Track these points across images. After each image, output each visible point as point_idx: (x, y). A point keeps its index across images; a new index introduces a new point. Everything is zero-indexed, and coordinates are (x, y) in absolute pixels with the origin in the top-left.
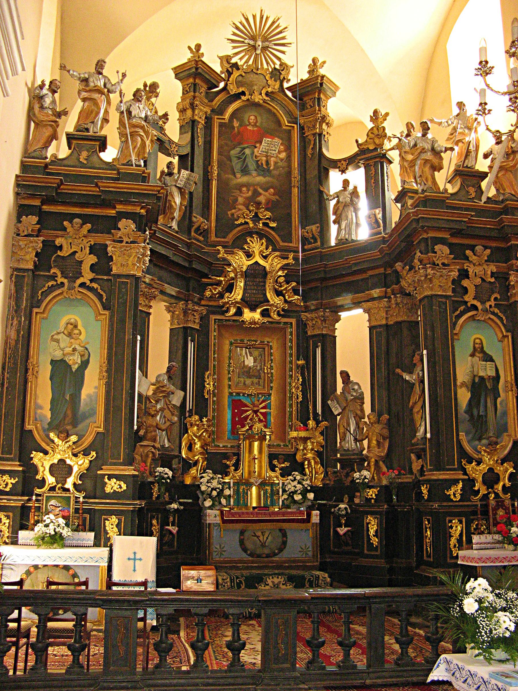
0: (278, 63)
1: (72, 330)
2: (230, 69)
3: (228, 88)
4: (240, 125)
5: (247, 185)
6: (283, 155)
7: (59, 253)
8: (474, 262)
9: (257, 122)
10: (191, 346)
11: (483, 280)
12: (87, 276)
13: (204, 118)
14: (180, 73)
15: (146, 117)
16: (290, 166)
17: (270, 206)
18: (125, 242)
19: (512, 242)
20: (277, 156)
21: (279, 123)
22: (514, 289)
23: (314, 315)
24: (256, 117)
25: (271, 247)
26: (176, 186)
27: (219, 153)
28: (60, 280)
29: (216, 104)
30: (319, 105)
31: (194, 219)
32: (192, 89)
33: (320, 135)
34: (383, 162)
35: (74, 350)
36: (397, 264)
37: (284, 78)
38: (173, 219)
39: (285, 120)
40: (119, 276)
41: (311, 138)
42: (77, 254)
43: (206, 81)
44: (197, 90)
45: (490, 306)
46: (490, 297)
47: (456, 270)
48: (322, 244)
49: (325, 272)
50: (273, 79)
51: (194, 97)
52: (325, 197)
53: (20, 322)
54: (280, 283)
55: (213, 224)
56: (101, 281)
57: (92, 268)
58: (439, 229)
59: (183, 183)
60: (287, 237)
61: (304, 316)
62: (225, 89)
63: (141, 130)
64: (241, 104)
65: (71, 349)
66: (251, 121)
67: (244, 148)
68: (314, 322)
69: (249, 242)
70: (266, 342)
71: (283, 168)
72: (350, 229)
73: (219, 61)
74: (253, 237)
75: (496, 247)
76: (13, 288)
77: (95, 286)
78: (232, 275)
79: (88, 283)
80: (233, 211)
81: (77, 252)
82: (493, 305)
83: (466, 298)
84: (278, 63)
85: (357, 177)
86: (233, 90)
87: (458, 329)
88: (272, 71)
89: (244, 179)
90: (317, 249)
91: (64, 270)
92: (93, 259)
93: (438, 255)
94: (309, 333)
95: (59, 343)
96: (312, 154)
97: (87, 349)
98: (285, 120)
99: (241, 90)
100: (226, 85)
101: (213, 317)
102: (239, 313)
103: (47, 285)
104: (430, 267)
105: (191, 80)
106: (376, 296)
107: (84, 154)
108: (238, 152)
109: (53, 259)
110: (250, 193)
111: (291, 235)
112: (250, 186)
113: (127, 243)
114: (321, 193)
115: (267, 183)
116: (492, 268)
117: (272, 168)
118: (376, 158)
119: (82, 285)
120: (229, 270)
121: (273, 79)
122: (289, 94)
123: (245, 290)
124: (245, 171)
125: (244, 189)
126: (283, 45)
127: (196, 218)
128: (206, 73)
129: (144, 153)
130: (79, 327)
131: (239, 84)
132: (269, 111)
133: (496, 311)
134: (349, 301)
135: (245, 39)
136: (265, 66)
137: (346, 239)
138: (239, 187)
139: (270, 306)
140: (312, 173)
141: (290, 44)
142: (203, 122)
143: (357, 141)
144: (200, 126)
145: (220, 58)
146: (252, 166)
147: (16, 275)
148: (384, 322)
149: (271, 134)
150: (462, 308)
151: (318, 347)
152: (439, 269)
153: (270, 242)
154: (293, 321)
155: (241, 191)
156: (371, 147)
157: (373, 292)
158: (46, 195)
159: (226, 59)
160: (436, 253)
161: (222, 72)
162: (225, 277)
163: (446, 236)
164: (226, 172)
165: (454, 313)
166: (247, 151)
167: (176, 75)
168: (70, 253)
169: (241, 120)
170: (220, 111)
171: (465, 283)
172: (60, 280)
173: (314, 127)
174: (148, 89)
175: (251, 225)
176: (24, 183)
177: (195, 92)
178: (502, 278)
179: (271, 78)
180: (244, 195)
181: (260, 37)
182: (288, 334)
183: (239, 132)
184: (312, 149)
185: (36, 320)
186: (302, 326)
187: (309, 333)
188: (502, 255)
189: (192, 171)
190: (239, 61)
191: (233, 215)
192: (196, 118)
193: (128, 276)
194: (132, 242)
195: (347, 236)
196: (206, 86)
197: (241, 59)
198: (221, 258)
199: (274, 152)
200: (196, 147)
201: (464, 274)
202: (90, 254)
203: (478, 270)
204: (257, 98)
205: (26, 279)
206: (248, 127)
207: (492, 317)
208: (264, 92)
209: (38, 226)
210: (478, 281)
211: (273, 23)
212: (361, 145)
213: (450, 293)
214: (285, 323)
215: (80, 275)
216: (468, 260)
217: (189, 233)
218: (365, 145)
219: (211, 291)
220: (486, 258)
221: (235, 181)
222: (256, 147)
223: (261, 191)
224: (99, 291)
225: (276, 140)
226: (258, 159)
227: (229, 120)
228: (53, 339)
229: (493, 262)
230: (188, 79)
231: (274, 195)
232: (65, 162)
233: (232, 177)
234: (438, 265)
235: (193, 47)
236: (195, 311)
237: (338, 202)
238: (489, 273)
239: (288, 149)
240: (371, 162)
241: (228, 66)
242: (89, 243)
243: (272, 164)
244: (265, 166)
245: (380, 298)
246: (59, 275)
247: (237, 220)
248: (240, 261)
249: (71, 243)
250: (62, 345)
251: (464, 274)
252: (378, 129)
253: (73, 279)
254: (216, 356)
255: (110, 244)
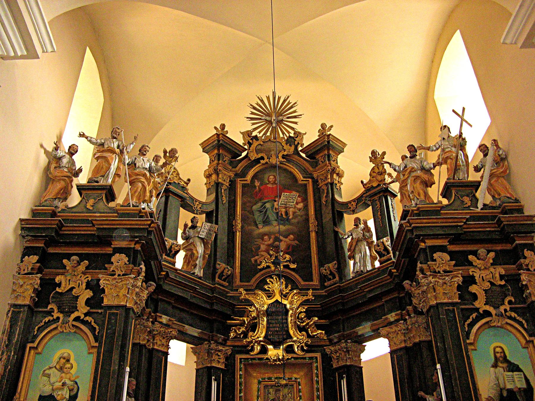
0: (292, 132)
1: (64, 364)
2: (251, 141)
3: (249, 155)
4: (261, 184)
5: (269, 234)
6: (301, 205)
7: (57, 289)
8: (479, 266)
9: (276, 180)
10: (214, 384)
11: (492, 284)
12: (82, 309)
13: (228, 181)
14: (206, 147)
15: (150, 167)
16: (307, 215)
17: (290, 250)
18: (117, 275)
19: (517, 242)
20: (295, 207)
21: (294, 178)
22: (528, 289)
23: (337, 347)
24: (275, 177)
25: (290, 286)
26: (198, 237)
27: (243, 209)
28: (56, 315)
29: (239, 170)
30: (329, 160)
31: (218, 266)
32: (216, 159)
33: (332, 184)
34: (387, 196)
35: (64, 384)
36: (404, 282)
37: (298, 143)
38: (195, 266)
39: (300, 176)
40: (110, 307)
41: (325, 188)
42: (74, 290)
43: (228, 151)
44: (221, 159)
45: (506, 310)
46: (503, 300)
47: (460, 275)
48: (341, 279)
49: (343, 304)
50: (288, 145)
51: (218, 164)
52: (341, 236)
53: (9, 356)
54: (302, 319)
55: (238, 270)
56: (96, 315)
57: (88, 302)
58: (436, 236)
59: (205, 234)
60: (308, 277)
61: (328, 350)
62: (246, 156)
63: (142, 178)
64: (261, 167)
65: (61, 384)
66: (270, 180)
67: (265, 203)
68: (338, 355)
69: (269, 282)
70: (293, 379)
71: (301, 216)
72: (365, 262)
73: (242, 136)
74: (273, 278)
75: (501, 250)
76: (8, 323)
77: (88, 319)
78: (254, 314)
79: (82, 317)
80: (257, 257)
81: (75, 288)
82: (508, 309)
83: (477, 304)
84: (292, 132)
85: (367, 215)
86: (254, 156)
87: (473, 338)
88: (287, 139)
89: (266, 229)
90: (336, 284)
91: (61, 305)
92: (89, 294)
93: (438, 263)
94: (334, 366)
95: (49, 378)
96: (326, 201)
97: (76, 383)
98: (300, 176)
99: (260, 156)
100: (248, 153)
101: (238, 357)
102: (264, 350)
103: (44, 321)
104: (430, 275)
105: (216, 151)
106: (392, 320)
107: (91, 202)
108: (259, 207)
109: (51, 295)
110: (272, 240)
111: (312, 275)
112: (271, 235)
113: (119, 275)
114: (336, 233)
115: (288, 230)
116: (500, 270)
117: (291, 217)
118: (379, 193)
119: (77, 319)
120: (251, 310)
121: (288, 145)
122: (304, 155)
123: (268, 328)
124: (266, 222)
125: (266, 237)
126: (295, 117)
127: (219, 265)
128: (226, 143)
129: (144, 196)
130: (71, 362)
131: (258, 151)
132: (286, 170)
133: (513, 314)
134: (368, 329)
135: (262, 116)
136: (281, 135)
137: (362, 271)
138: (262, 236)
139: (294, 342)
140: (327, 217)
141: (301, 115)
142: (228, 185)
143: (362, 182)
144: (224, 187)
145: (242, 133)
146: (272, 216)
147: (13, 311)
148: (403, 345)
149: (286, 188)
150: (474, 315)
151: (343, 378)
152: (442, 276)
153: (289, 281)
154: (318, 355)
155: (263, 240)
156: (375, 185)
157: (389, 316)
158: (49, 237)
159: (247, 134)
160: (435, 260)
161: (245, 144)
162: (248, 317)
163: (444, 244)
164: (250, 225)
165: (465, 321)
166: (268, 205)
167: (203, 149)
168: (68, 289)
169: (261, 180)
170: (243, 174)
171: (473, 289)
172: (56, 315)
173: (326, 178)
174: (168, 154)
175: (273, 268)
176: (27, 226)
177: (219, 160)
178: (513, 280)
179: (287, 144)
180: (266, 243)
181: (275, 114)
182: (314, 368)
183: (260, 190)
184: (326, 197)
185: (30, 357)
186: (327, 359)
187: (334, 366)
188: (511, 257)
189: (217, 223)
190: (258, 134)
191: (256, 261)
192: (220, 180)
193: (118, 307)
194: (123, 275)
195: (362, 268)
196: (230, 156)
197: (260, 132)
198: (243, 299)
199: (292, 204)
200: (220, 205)
201: (470, 280)
202: (86, 289)
203: (484, 273)
204: (273, 161)
205: (21, 315)
206: (269, 186)
207: (509, 321)
208: (280, 155)
209: (38, 265)
210: (487, 285)
211: (285, 101)
212: (366, 184)
213: (457, 300)
214: (311, 358)
215: (75, 309)
216: (473, 265)
217: (213, 279)
218: (369, 184)
219: (235, 331)
220: (491, 261)
221: (257, 232)
222: (275, 201)
223: (281, 238)
224: (93, 323)
225: (294, 193)
226: (277, 211)
227: (251, 181)
228: (44, 375)
229: (500, 265)
230: (213, 151)
231: (294, 240)
232: (74, 210)
233: (255, 228)
234: (439, 272)
235: (218, 127)
236: (219, 351)
237: (352, 239)
238: (497, 275)
239: (305, 200)
240: (376, 198)
241: (249, 139)
242: (87, 279)
243: (291, 213)
244: (284, 216)
245: (397, 321)
246: (56, 310)
247: (259, 265)
248: (262, 302)
249: (69, 280)
250: (53, 380)
251: (470, 280)
252: (378, 168)
253: (68, 314)
254: (242, 394)
255: (103, 277)
